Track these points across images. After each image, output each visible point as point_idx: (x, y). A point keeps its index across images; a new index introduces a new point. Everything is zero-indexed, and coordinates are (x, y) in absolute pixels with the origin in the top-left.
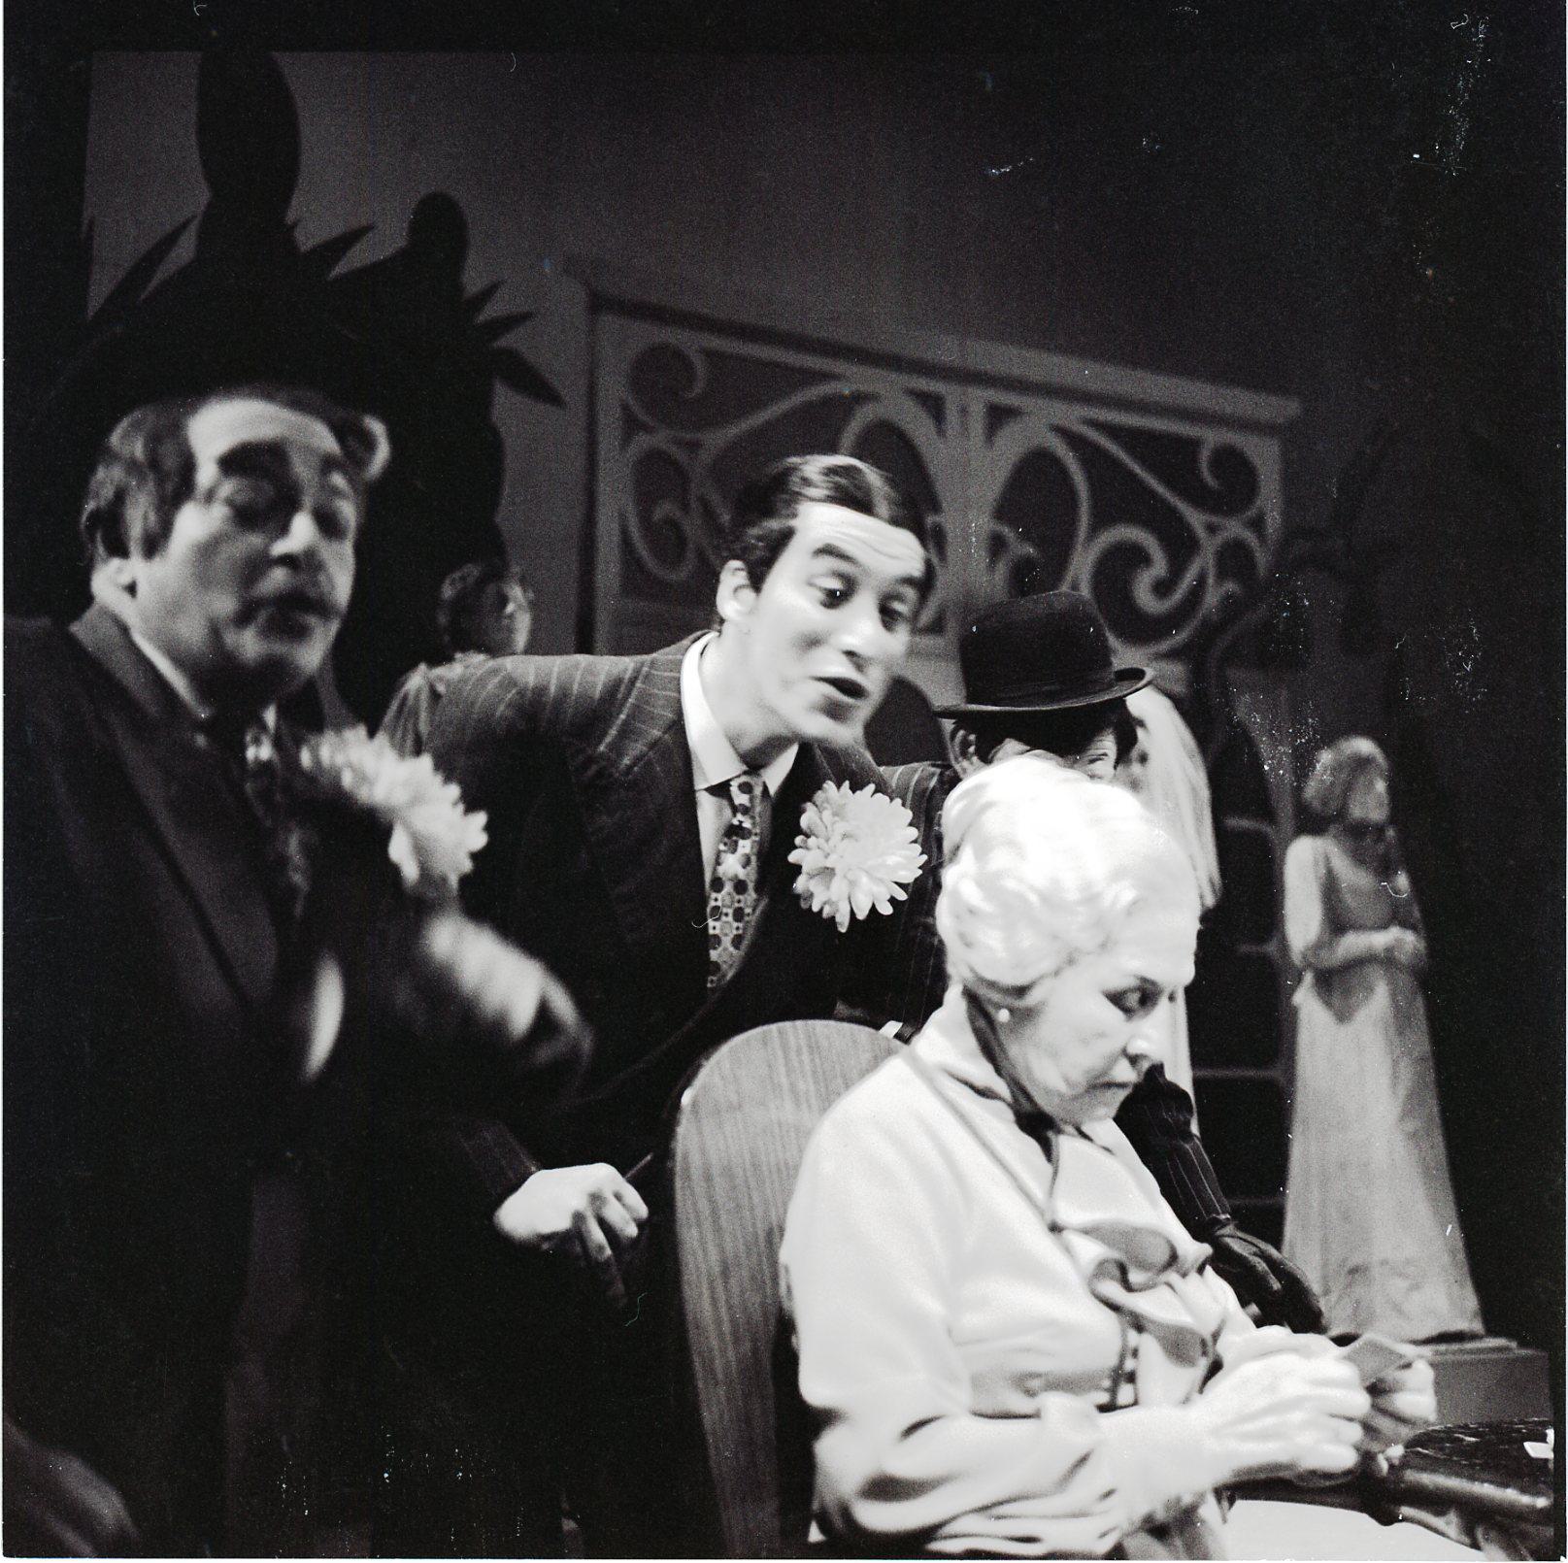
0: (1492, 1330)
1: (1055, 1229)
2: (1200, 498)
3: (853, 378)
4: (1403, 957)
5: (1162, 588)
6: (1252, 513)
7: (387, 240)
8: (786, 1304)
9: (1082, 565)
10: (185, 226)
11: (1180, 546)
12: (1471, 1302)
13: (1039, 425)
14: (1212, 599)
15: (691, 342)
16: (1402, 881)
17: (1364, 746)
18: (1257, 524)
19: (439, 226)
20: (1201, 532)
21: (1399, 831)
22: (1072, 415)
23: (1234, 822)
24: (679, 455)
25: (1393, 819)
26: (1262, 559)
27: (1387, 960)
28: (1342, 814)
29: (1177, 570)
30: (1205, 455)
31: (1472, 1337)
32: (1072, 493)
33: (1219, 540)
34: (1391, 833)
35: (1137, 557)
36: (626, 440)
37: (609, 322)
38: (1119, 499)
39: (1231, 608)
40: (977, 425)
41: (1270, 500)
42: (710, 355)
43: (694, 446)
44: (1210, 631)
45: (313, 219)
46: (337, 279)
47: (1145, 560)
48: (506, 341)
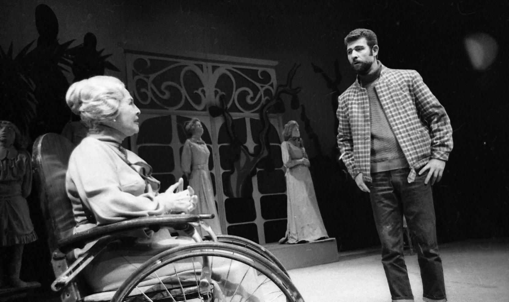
0: (330, 237)
1: (130, 164)
2: (260, 81)
3: (183, 62)
4: (305, 164)
5: (252, 99)
6: (270, 83)
7: (79, 41)
8: (88, 206)
9: (235, 95)
10: (34, 41)
11: (256, 90)
12: (325, 231)
13: (222, 69)
14: (264, 100)
15: (146, 58)
16: (304, 149)
17: (294, 122)
18: (272, 85)
19: (90, 39)
20: (260, 88)
21: (303, 139)
22: (230, 67)
23: (403, 275)
24: (145, 79)
25: (301, 136)
26: (273, 92)
27: (303, 164)
28: (290, 136)
29: (255, 95)
30: (259, 73)
31: (327, 238)
32: (232, 82)
33: (264, 88)
34: (301, 139)
35: (246, 93)
36: (134, 76)
37: (129, 55)
38: (241, 82)
39: (268, 101)
40: (210, 70)
41: (274, 80)
42: (150, 60)
43: (148, 78)
44: (263, 106)
45: (62, 38)
46: (229, 169)
47: (249, 94)
48: (107, 60)
